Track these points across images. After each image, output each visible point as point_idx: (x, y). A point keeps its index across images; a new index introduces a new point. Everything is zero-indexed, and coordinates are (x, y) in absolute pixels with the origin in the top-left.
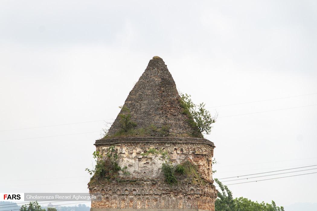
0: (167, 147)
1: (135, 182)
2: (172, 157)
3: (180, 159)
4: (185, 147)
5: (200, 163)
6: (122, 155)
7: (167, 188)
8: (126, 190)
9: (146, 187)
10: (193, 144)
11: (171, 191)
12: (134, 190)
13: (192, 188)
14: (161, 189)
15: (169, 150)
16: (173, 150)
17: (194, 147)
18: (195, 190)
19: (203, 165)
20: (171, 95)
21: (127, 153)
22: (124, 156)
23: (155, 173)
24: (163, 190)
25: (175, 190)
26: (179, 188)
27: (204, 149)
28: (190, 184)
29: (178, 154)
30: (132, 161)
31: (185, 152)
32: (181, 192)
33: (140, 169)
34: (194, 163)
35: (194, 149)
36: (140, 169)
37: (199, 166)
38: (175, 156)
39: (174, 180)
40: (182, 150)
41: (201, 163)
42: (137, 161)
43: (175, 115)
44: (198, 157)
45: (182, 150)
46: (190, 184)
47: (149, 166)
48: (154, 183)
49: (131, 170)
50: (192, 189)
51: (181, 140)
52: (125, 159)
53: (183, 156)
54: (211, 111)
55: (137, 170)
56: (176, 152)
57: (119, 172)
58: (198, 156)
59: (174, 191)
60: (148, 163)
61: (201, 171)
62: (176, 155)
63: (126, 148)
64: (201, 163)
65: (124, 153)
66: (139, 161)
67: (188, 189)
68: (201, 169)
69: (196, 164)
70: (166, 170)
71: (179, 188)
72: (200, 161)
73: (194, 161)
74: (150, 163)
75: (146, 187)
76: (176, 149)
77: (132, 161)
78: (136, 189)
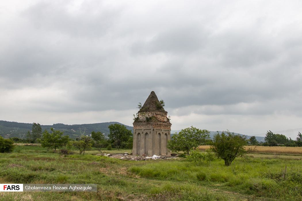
1: (141, 122)
17: (156, 112)
37: (157, 117)
38: (150, 114)
40: (152, 113)
41: (158, 116)
45: (152, 113)
49: (141, 119)
64: (158, 116)
67: (151, 123)
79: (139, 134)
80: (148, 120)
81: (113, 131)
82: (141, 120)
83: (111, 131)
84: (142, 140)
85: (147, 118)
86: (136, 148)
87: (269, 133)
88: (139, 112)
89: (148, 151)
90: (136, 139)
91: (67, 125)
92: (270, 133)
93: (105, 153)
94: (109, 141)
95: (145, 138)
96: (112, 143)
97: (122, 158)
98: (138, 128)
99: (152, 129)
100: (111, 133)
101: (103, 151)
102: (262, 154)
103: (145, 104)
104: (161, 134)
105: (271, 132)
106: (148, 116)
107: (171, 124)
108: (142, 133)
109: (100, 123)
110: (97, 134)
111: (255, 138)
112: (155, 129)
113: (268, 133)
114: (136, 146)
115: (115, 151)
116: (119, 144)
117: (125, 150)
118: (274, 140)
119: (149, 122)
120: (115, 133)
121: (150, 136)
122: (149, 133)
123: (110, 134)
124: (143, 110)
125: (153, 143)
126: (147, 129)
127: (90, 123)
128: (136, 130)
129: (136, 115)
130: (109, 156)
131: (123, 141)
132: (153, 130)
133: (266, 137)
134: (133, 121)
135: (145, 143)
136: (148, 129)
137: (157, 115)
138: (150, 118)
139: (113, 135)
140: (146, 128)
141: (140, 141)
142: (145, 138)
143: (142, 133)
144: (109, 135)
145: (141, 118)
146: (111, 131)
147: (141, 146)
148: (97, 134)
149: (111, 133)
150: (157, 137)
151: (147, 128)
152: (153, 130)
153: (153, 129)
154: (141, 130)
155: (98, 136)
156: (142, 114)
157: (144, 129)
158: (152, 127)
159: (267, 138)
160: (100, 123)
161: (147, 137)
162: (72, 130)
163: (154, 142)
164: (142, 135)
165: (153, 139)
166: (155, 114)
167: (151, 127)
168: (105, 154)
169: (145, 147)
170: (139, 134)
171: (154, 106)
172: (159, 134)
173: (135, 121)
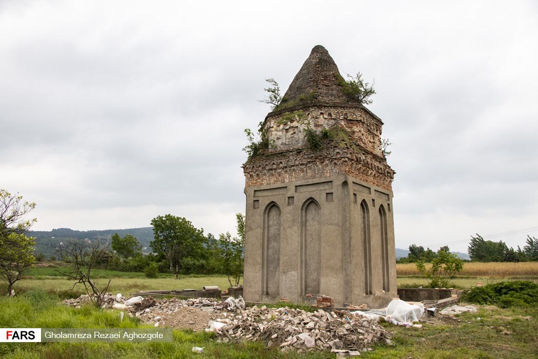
0: (311, 112)
1: (282, 154)
2: (318, 122)
3: (328, 124)
4: (333, 111)
5: (355, 129)
6: (271, 129)
7: (312, 155)
8: (274, 164)
9: (291, 158)
10: (344, 108)
11: (316, 158)
12: (281, 163)
13: (338, 151)
14: (306, 157)
15: (314, 114)
16: (319, 114)
17: (346, 111)
18: (341, 152)
19: (358, 131)
20: (326, 71)
21: (275, 126)
22: (273, 129)
23: (300, 141)
24: (308, 158)
25: (320, 156)
26: (324, 153)
27: (358, 114)
28: (336, 147)
29: (326, 119)
30: (280, 134)
31: (334, 116)
32: (326, 157)
33: (287, 140)
34: (347, 129)
35: (346, 114)
36: (287, 140)
37: (354, 132)
38: (321, 120)
39: (319, 144)
40: (330, 115)
41: (356, 129)
42: (285, 133)
43: (328, 86)
44: (352, 123)
45: (330, 115)
46: (336, 147)
47: (295, 136)
48: (299, 152)
49: (279, 143)
50: (338, 152)
51: (327, 104)
52: (273, 133)
53: (333, 121)
54: (368, 81)
55: (284, 141)
56: (323, 117)
57: (476, 311)
58: (352, 122)
59: (319, 158)
60: (294, 133)
61: (356, 138)
62: (323, 119)
63: (274, 121)
64: (356, 129)
65: (273, 127)
66: (287, 132)
67: (333, 153)
68: (356, 136)
69: (349, 130)
70: (310, 135)
71: (324, 153)
72: (355, 127)
73: (346, 126)
74: (297, 132)
75: (291, 158)
76: (322, 114)
77: (280, 134)
78: (282, 161)
79: (272, 205)
80: (317, 145)
81: (161, 232)
82: (284, 148)
83: (157, 233)
84: (288, 230)
85: (310, 135)
86: (260, 266)
87: (474, 240)
88: (270, 116)
89: (323, 281)
90: (260, 231)
91: (78, 231)
92: (477, 238)
93: (119, 289)
94: (151, 258)
95: (304, 224)
96: (159, 261)
97: (217, 326)
98: (267, 181)
99: (338, 182)
100: (157, 238)
101: (101, 283)
102: (417, 277)
103: (294, 88)
104: (369, 203)
105: (480, 237)
106: (316, 126)
107: (394, 173)
108: (289, 204)
109: (139, 227)
110: (124, 242)
111: (448, 250)
112: (351, 179)
113: (472, 239)
114: (259, 260)
115: (168, 279)
116: (176, 263)
117: (194, 277)
118: (484, 251)
119: (324, 153)
120: (166, 238)
121: (329, 210)
122: (321, 198)
123: (154, 240)
124: (284, 110)
125: (344, 243)
126: (311, 181)
127: (119, 229)
128: (258, 194)
129: (255, 129)
130: (138, 307)
131: (187, 257)
132: (345, 183)
133: (470, 246)
134: (245, 157)
135: (304, 246)
136: (316, 180)
137: (350, 121)
138: (325, 135)
139: (161, 241)
140: (304, 178)
141: (277, 237)
142: (304, 224)
143: (289, 204)
144: (151, 242)
145: (279, 136)
146: (157, 233)
147: (283, 259)
148: (124, 242)
149: (158, 238)
150: (357, 211)
151: (314, 177)
152: (345, 183)
153: (342, 179)
154: (281, 192)
155: (127, 245)
156: (286, 124)
157: (299, 183)
158: (336, 170)
159: (472, 251)
160: (138, 229)
161: (309, 217)
162: (86, 240)
163: (350, 238)
164: (288, 213)
165: (345, 227)
166: (345, 119)
167: (329, 172)
168: (119, 296)
169: (305, 264)
170: (272, 205)
171: (335, 92)
172: (364, 204)
173: (251, 159)
